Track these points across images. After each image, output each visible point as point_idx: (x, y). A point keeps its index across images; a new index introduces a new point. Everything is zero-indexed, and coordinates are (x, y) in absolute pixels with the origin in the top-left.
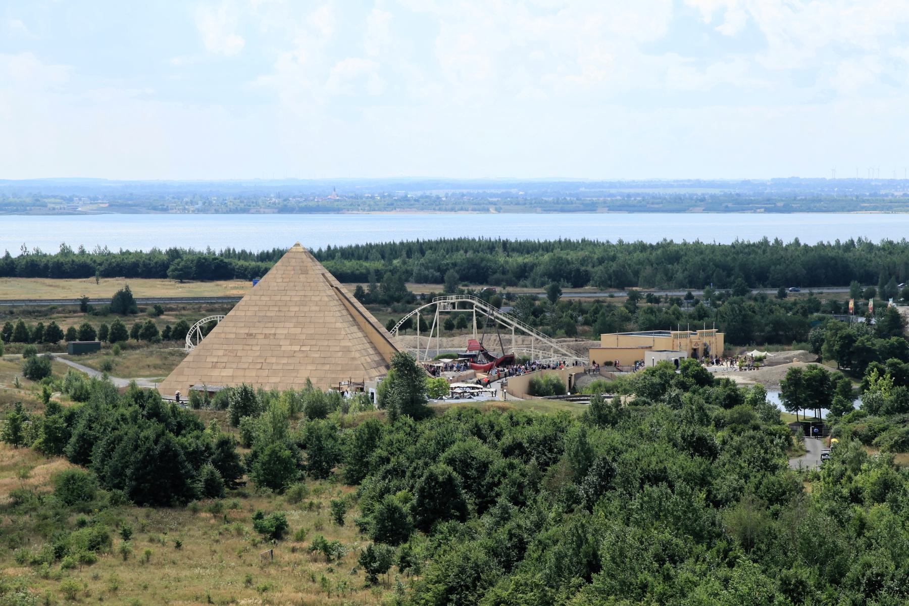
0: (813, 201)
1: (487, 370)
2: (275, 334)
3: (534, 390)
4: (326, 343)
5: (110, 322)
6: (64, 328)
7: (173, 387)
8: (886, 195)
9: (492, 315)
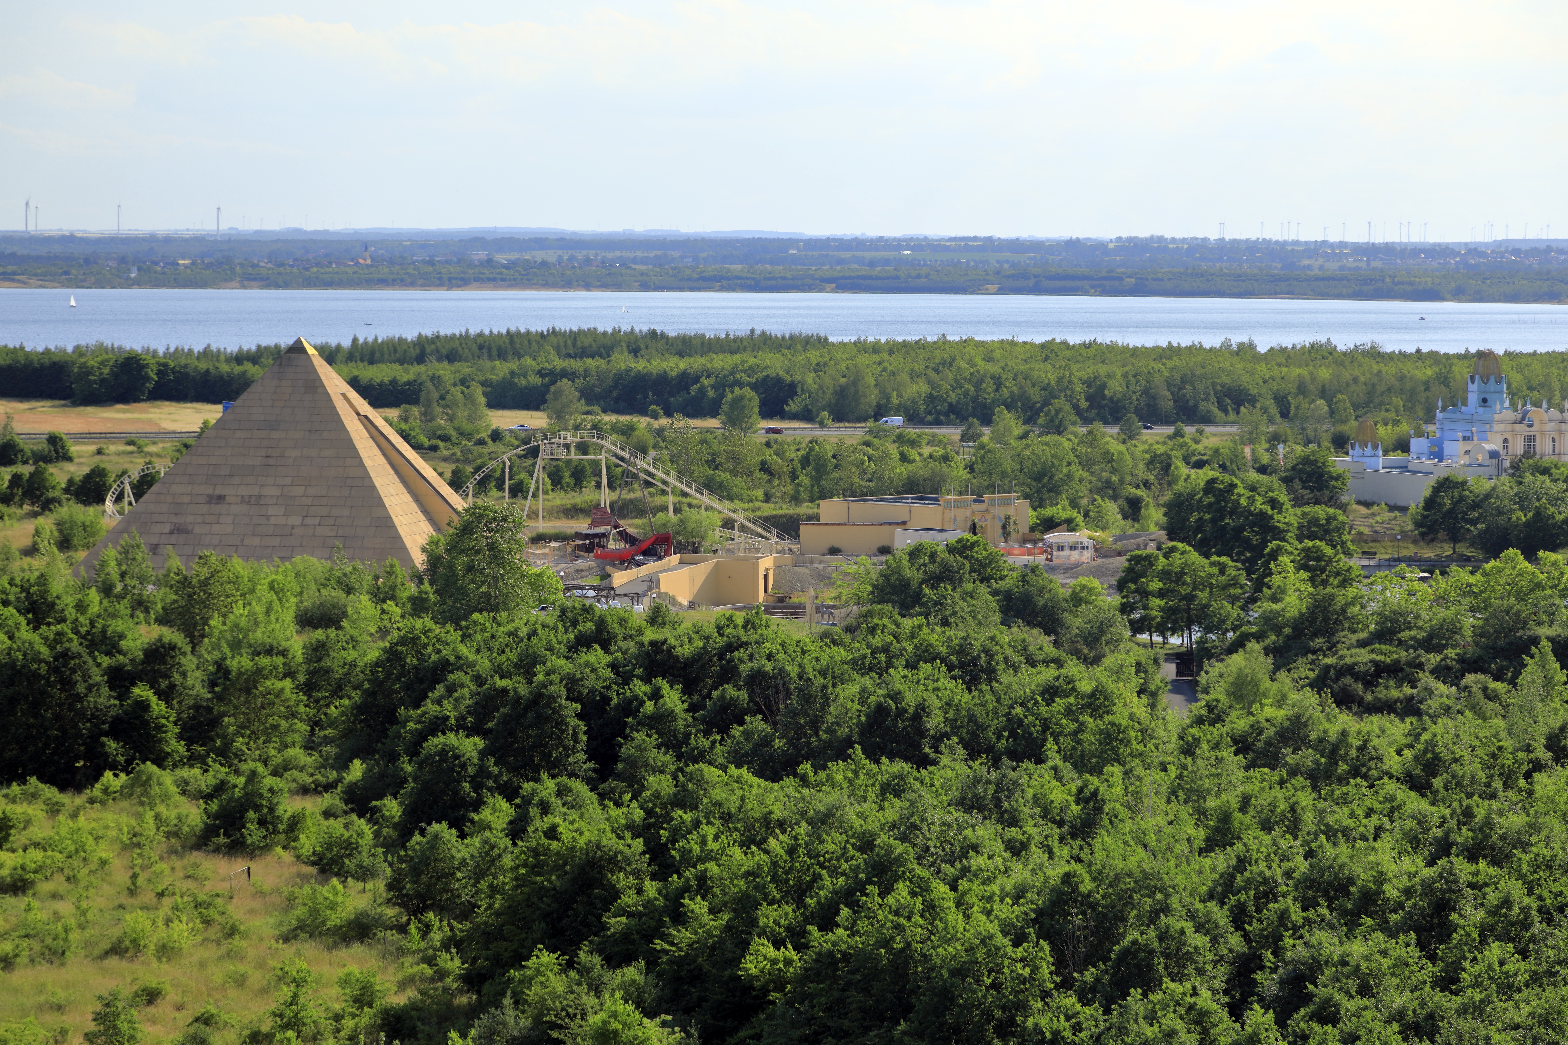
2: (259, 497)
4: (346, 512)
8: (1309, 267)
9: (635, 466)
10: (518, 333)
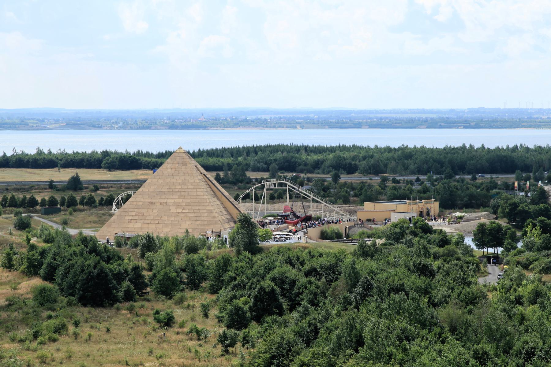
0: (493, 122)
1: (295, 224)
2: (167, 202)
3: (324, 236)
4: (198, 208)
5: (67, 195)
6: (39, 198)
7: (105, 234)
8: (537, 118)
9: (298, 191)
10: (257, 147)
